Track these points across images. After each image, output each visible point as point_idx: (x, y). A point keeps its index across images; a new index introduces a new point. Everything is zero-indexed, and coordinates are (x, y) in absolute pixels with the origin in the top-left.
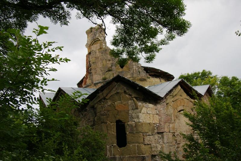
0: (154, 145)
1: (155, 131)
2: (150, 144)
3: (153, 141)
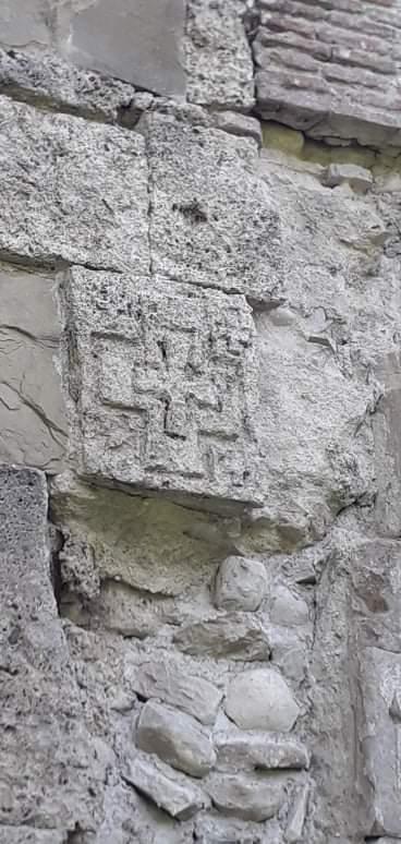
0: (157, 291)
1: (206, 64)
2: (53, 265)
3: (130, 223)
